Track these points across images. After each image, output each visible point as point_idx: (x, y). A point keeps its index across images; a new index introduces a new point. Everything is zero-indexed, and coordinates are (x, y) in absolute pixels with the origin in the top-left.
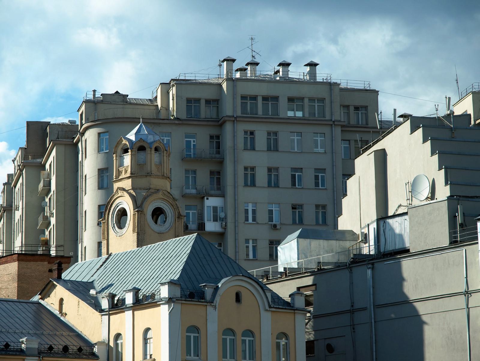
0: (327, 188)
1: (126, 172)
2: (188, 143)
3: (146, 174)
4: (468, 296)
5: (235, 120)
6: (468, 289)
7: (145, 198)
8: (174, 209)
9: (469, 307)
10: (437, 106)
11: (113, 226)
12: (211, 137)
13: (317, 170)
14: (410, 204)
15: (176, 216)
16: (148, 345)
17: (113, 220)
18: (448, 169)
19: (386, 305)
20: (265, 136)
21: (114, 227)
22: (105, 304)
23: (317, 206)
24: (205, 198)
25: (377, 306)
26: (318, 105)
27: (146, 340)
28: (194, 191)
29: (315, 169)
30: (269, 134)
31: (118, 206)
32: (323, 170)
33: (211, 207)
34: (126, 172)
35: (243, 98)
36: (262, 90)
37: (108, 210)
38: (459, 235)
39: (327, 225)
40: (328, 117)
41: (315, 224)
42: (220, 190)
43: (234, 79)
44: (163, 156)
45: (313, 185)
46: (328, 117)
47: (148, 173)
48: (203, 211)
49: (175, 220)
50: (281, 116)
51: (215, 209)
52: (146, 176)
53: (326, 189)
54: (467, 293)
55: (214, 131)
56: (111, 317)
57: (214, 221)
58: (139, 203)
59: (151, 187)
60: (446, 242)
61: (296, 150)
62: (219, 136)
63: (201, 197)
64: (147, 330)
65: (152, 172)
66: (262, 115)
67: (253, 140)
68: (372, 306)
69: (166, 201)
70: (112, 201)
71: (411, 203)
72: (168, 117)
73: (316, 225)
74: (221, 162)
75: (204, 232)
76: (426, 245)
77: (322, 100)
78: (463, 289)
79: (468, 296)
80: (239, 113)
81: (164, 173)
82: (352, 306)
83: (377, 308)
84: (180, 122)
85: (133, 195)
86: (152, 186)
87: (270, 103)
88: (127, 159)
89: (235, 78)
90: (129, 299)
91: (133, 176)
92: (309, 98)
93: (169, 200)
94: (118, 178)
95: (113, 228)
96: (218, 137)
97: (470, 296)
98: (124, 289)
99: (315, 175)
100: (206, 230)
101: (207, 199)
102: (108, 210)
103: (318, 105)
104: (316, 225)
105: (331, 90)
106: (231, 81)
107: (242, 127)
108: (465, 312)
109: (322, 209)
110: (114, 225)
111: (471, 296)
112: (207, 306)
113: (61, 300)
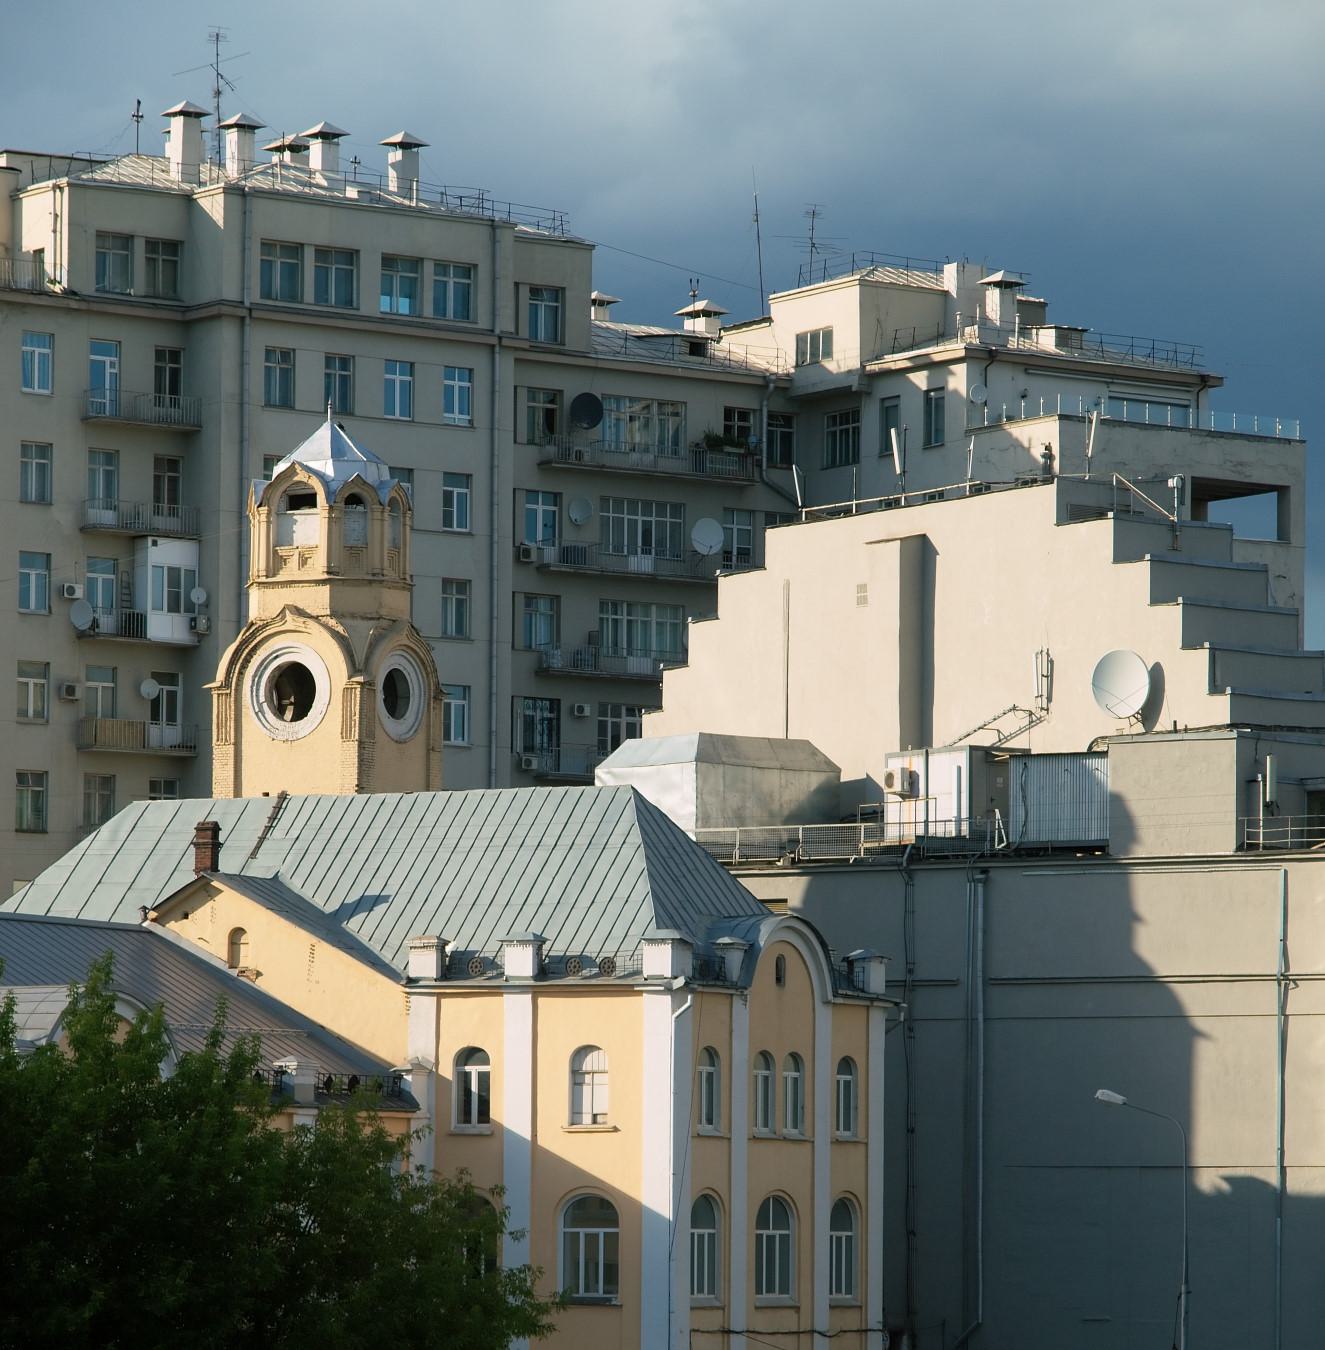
0: (474, 533)
1: (303, 561)
2: (97, 369)
3: (370, 577)
4: (1286, 986)
5: (244, 316)
6: (1287, 968)
7: (373, 646)
8: (427, 674)
9: (1287, 1013)
10: (694, 282)
11: (257, 710)
12: (159, 354)
13: (451, 478)
14: (1042, 709)
15: (430, 695)
16: (586, 1090)
17: (258, 690)
18: (1217, 652)
19: (1025, 982)
20: (320, 370)
21: (261, 710)
22: (424, 965)
23: (447, 583)
24: (150, 540)
25: (990, 982)
26: (455, 283)
27: (577, 1076)
28: (108, 517)
29: (445, 473)
30: (329, 360)
31: (277, 657)
32: (466, 479)
33: (162, 567)
34: (303, 561)
35: (267, 246)
36: (317, 230)
37: (241, 661)
38: (1261, 830)
39: (469, 639)
40: (483, 323)
41: (440, 635)
42: (177, 516)
43: (246, 189)
44: (405, 525)
45: (439, 525)
46: (483, 323)
47: (374, 575)
48: (133, 577)
49: (429, 704)
50: (364, 311)
51: (174, 573)
52: (370, 582)
53: (470, 534)
54: (1286, 980)
55: (167, 339)
56: (443, 1001)
57: (170, 610)
58: (360, 657)
59: (382, 613)
60: (1228, 847)
61: (397, 415)
62: (179, 352)
63: (134, 538)
64: (583, 1051)
65: (385, 572)
66: (315, 305)
67: (287, 377)
68: (980, 981)
69: (414, 655)
70: (258, 639)
71: (1045, 706)
72: (42, 282)
73: (442, 638)
74: (189, 435)
75: (144, 641)
76: (1162, 844)
77: (468, 270)
78: (1275, 968)
79: (1286, 986)
80: (254, 296)
81: (404, 573)
82: (910, 971)
83: (993, 984)
84: (83, 306)
85: (338, 632)
86: (384, 612)
87: (334, 267)
88: (312, 528)
89: (250, 188)
90: (519, 963)
91: (334, 577)
92: (435, 260)
93: (418, 650)
94: (274, 575)
95: (256, 714)
96: (175, 355)
97: (1292, 985)
98: (380, 909)
99: (445, 492)
100: (148, 637)
101: (155, 543)
102: (241, 661)
103: (455, 283)
104: (442, 638)
105: (494, 241)
106: (724, 1322)
107: (261, 338)
108: (1274, 1025)
109: (458, 592)
110: (260, 705)
111: (1297, 986)
112: (734, 998)
113: (236, 935)
